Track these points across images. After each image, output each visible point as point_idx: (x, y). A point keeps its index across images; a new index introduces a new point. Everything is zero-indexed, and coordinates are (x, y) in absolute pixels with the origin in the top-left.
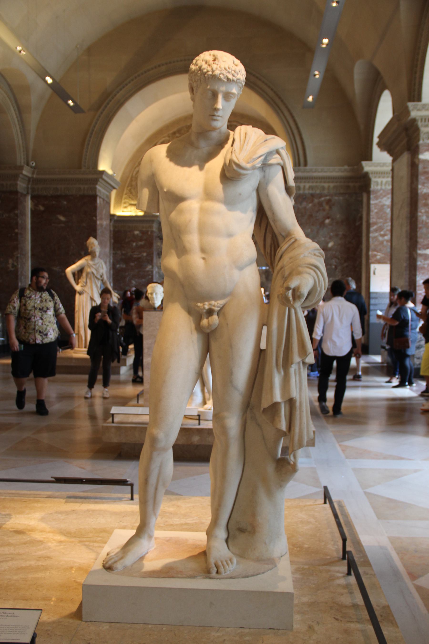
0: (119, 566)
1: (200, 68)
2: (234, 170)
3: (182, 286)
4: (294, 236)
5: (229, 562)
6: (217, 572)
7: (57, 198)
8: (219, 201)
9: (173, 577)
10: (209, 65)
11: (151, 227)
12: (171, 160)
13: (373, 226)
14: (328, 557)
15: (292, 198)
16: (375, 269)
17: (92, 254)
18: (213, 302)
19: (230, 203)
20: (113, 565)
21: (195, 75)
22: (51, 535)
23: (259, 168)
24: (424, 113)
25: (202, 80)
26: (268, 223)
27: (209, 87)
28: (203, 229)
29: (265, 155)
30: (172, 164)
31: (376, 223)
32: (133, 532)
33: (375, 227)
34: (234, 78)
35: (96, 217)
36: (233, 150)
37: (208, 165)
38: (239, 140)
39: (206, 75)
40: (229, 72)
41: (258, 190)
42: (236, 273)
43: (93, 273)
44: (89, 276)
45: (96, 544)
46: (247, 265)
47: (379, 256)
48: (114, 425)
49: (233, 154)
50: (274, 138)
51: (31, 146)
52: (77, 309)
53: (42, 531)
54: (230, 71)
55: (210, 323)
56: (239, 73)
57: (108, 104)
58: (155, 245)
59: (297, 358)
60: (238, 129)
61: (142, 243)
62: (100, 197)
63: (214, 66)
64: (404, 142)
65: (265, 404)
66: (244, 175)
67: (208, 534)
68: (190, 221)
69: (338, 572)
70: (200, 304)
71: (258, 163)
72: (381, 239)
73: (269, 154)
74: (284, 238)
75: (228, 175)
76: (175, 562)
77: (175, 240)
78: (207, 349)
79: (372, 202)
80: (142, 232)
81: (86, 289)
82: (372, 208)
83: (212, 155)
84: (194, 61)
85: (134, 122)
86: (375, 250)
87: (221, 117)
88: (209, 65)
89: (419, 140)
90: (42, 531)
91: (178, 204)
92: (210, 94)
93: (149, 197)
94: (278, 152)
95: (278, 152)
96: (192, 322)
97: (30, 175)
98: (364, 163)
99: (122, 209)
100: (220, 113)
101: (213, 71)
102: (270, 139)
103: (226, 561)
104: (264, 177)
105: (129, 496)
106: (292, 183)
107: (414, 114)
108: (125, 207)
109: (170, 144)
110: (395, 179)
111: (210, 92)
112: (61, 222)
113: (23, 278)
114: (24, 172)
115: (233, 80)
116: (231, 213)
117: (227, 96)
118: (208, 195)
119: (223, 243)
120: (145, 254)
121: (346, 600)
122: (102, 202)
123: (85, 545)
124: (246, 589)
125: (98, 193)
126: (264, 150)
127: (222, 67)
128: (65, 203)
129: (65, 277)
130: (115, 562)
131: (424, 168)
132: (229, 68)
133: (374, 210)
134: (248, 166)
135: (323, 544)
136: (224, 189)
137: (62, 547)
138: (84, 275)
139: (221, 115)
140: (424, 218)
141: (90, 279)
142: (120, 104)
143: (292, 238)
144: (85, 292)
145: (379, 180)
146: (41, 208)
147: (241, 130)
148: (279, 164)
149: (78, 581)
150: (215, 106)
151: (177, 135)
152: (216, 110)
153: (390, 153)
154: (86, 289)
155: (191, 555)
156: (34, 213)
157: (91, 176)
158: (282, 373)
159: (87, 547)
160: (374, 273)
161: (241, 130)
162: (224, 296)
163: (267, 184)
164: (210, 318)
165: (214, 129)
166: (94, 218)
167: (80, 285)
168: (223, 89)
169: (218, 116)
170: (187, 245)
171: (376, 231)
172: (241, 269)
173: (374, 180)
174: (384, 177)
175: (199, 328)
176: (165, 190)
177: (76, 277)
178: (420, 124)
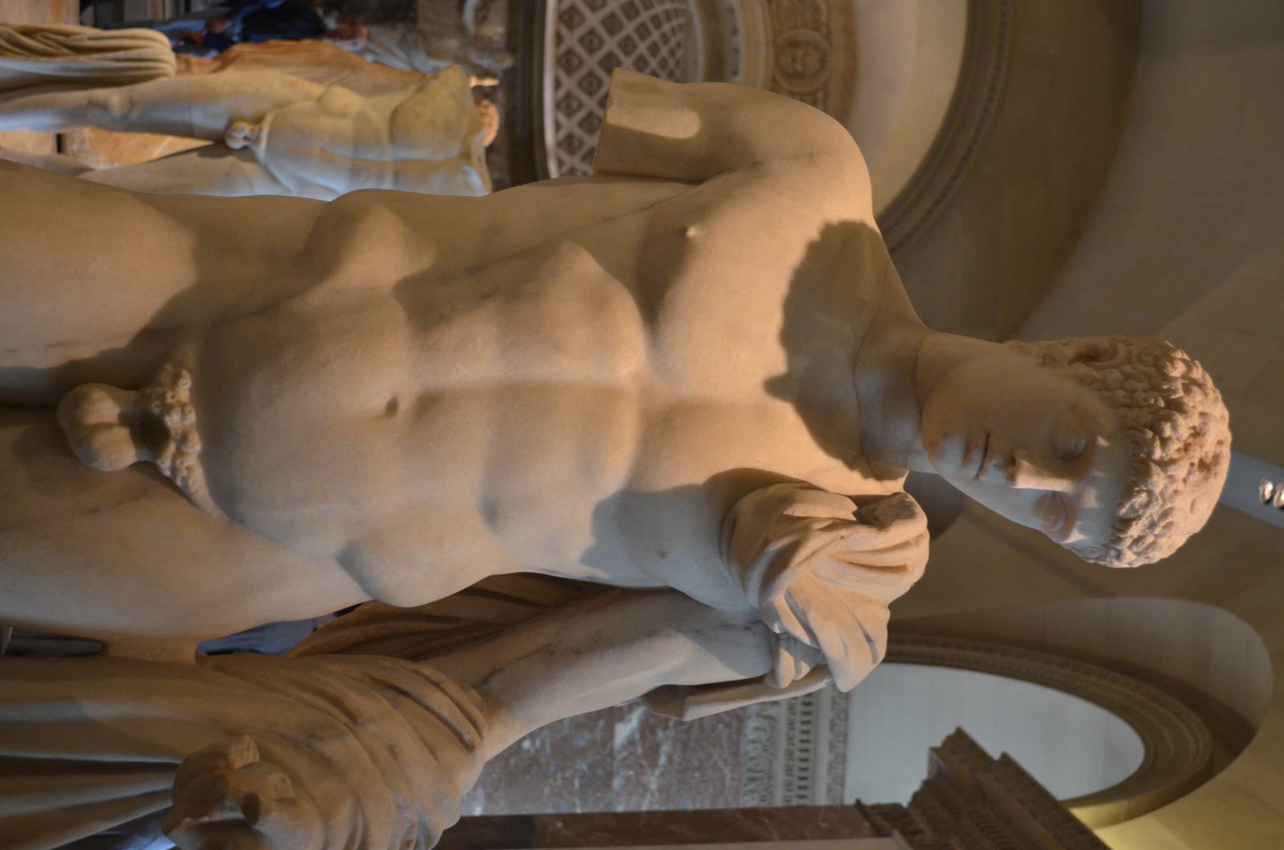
1: (1177, 407)
2: (767, 542)
8: (640, 468)
10: (1186, 448)
12: (814, 249)
18: (195, 446)
19: (629, 512)
21: (1149, 377)
25: (1135, 411)
27: (1102, 442)
28: (520, 404)
30: (794, 255)
34: (1129, 542)
37: (786, 413)
38: (881, 546)
39: (1150, 434)
40: (1152, 525)
42: (333, 542)
46: (361, 580)
54: (1157, 531)
63: (1180, 471)
66: (744, 581)
68: (557, 347)
70: (184, 390)
75: (746, 505)
77: (476, 269)
84: (1198, 373)
87: (978, 475)
88: (1186, 448)
91: (632, 290)
94: (821, 668)
96: (105, 347)
100: (993, 476)
104: (727, 626)
109: (872, 231)
111: (1082, 445)
115: (1119, 540)
116: (584, 515)
118: (666, 422)
119: (461, 484)
134: (779, 600)
136: (687, 492)
139: (982, 478)
150: (1025, 464)
152: (1010, 466)
162: (227, 495)
163: (697, 634)
164: (122, 433)
168: (1091, 500)
169: (982, 468)
170: (451, 335)
172: (348, 560)
176: (692, 232)
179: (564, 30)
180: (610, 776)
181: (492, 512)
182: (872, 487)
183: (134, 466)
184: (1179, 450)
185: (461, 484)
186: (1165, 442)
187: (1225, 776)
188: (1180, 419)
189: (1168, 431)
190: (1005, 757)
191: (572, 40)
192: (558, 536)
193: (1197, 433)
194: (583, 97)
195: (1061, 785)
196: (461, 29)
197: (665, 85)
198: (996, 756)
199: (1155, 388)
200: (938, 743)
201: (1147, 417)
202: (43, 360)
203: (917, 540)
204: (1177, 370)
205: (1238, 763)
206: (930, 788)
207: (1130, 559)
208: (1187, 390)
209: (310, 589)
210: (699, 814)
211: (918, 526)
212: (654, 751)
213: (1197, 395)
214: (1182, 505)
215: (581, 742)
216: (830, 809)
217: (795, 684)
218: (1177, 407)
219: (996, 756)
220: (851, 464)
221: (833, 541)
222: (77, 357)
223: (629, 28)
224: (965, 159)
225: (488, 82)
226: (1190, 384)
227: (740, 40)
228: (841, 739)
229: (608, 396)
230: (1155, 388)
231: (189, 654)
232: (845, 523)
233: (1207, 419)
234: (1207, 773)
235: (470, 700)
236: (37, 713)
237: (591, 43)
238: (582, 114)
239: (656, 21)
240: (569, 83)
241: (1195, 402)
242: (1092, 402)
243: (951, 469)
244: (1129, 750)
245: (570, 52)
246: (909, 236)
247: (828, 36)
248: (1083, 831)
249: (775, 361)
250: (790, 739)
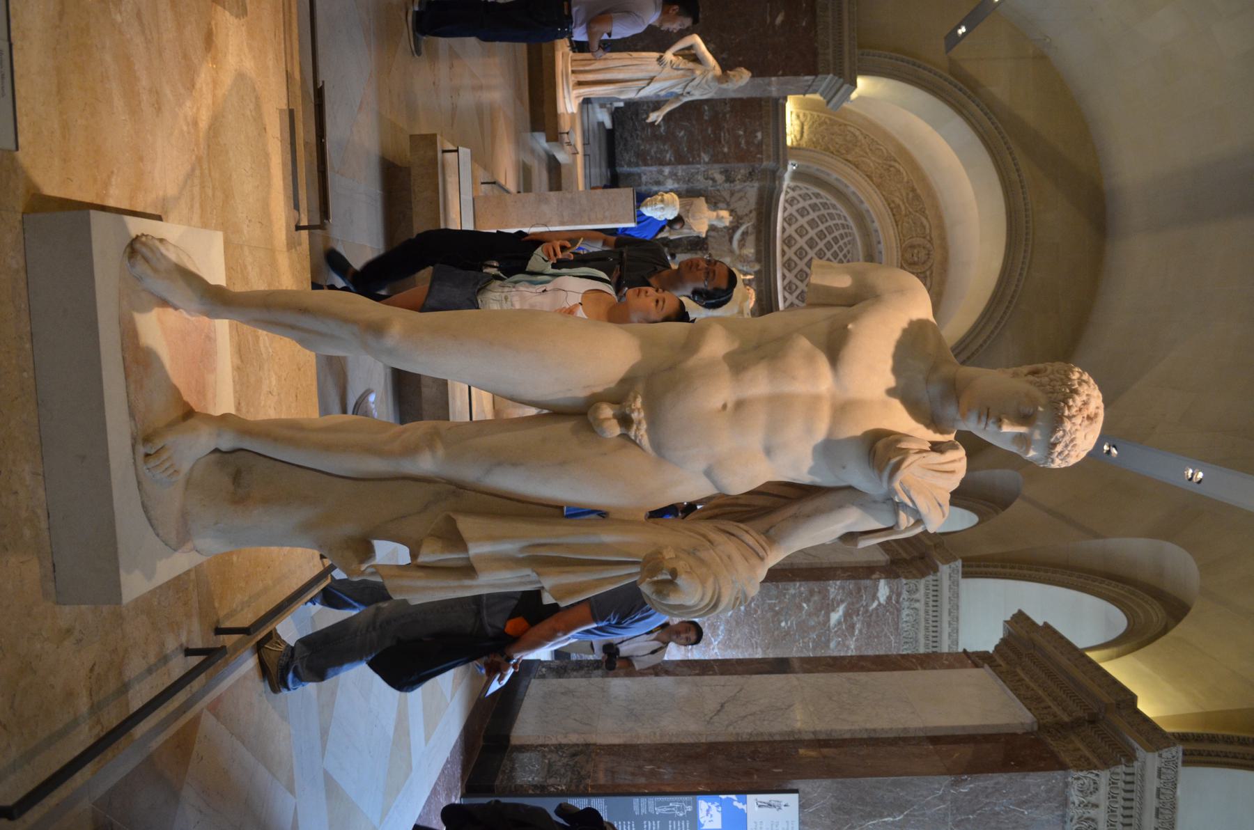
0: (141, 267)
1: (1075, 392)
5: (171, 471)
6: (147, 455)
8: (831, 431)
9: (127, 377)
10: (1080, 410)
11: (768, 157)
12: (906, 332)
14: (217, 605)
17: (724, 78)
18: (644, 426)
19: (829, 449)
20: (139, 257)
22: (208, 100)
24: (946, 583)
27: (1040, 409)
28: (779, 404)
30: (896, 335)
32: (216, 275)
37: (896, 404)
40: (1066, 446)
41: (850, 488)
42: (701, 466)
44: (689, 73)
45: (197, 190)
46: (714, 482)
48: (439, 154)
52: (635, 54)
53: (215, 83)
57: (960, 90)
58: (741, 165)
61: (743, 145)
63: (1078, 420)
64: (904, 555)
65: (466, 525)
66: (880, 478)
67: (225, 417)
68: (794, 378)
69: (189, 632)
74: (766, 533)
75: (880, 444)
76: (162, 367)
77: (758, 347)
78: (556, 413)
80: (761, 143)
84: (1086, 376)
85: (930, 128)
88: (1080, 410)
89: (906, 578)
90: (215, 83)
92: (1027, 410)
93: (836, 289)
94: (919, 521)
99: (795, 111)
100: (992, 427)
101: (1070, 418)
103: (172, 465)
104: (875, 502)
105: (304, 222)
107: (945, 569)
108: (798, 116)
112: (774, 18)
115: (1052, 453)
118: (842, 409)
120: (726, 150)
121: (135, 666)
123: (193, 170)
124: (118, 517)
125: (820, 77)
130: (146, 260)
131: (866, 588)
134: (897, 485)
135: (242, 584)
137: (185, 128)
138: (691, 65)
140: (792, 591)
141: (684, 76)
142: (959, 109)
148: (897, 524)
149: (113, 180)
150: (1006, 421)
151: (911, 195)
152: (999, 422)
154: (668, 68)
155: (182, 391)
157: (846, 64)
158: (521, 556)
159: (190, 175)
163: (862, 506)
164: (615, 422)
167: (673, 58)
168: (1037, 435)
170: (748, 375)
172: (708, 473)
175: (593, 401)
176: (850, 326)
178: (931, 578)
179: (786, 248)
180: (828, 641)
181: (768, 451)
182: (938, 438)
183: (620, 435)
185: (755, 440)
186: (1069, 408)
187: (1173, 633)
188: (1077, 397)
189: (1071, 403)
190: (1045, 623)
191: (790, 253)
192: (796, 463)
193: (1085, 403)
194: (798, 283)
195: (1080, 643)
196: (732, 252)
197: (835, 264)
198: (1040, 623)
199: (1065, 384)
200: (1008, 619)
201: (1061, 397)
202: (581, 393)
203: (960, 459)
204: (1075, 376)
205: (1180, 626)
206: (1005, 643)
207: (1058, 464)
208: (1080, 384)
209: (690, 486)
210: (878, 657)
211: (961, 453)
212: (852, 627)
213: (1085, 386)
214: (1081, 437)
215: (812, 623)
216: (949, 654)
217: (907, 529)
218: (1075, 392)
219: (1040, 623)
220: (928, 426)
223: (821, 245)
224: (1010, 302)
225: (749, 277)
226: (1081, 382)
227: (882, 247)
228: (955, 619)
229: (816, 399)
230: (1065, 384)
232: (926, 451)
233: (1089, 399)
234: (1165, 631)
235: (762, 539)
236: (583, 539)
237: (801, 253)
238: (798, 292)
239: (836, 240)
240: (790, 276)
241: (1084, 389)
242: (1036, 392)
243: (971, 425)
244: (1118, 621)
245: (790, 259)
246: (981, 346)
247: (930, 241)
248: (1091, 661)
249: (890, 381)
250: (926, 620)
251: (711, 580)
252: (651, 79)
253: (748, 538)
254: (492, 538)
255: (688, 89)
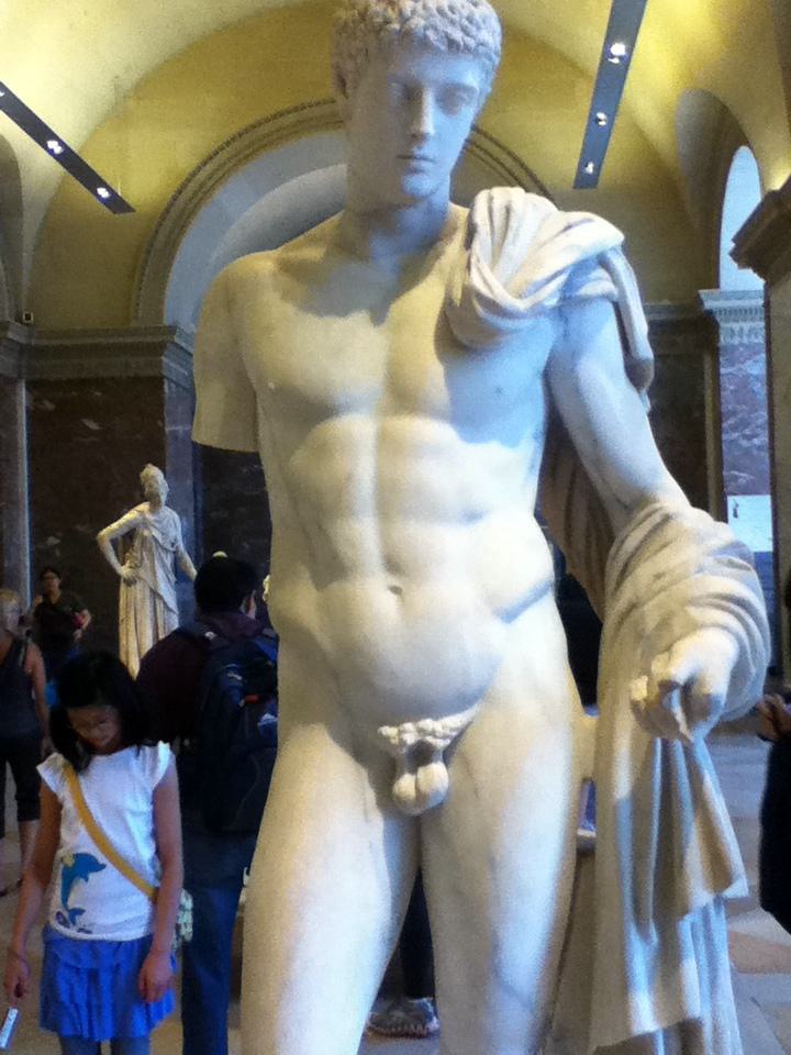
1: (363, 16)
2: (478, 318)
3: (336, 676)
4: (657, 505)
7: (82, 383)
8: (436, 414)
13: (728, 419)
15: (644, 391)
16: (737, 505)
18: (428, 724)
19: (469, 419)
23: (553, 309)
26: (577, 470)
29: (569, 272)
31: (734, 413)
33: (731, 421)
34: (468, 39)
35: (163, 420)
36: (473, 260)
40: (452, 22)
41: (547, 377)
42: (496, 632)
43: (156, 540)
46: (525, 605)
47: (744, 477)
49: (474, 270)
50: (590, 220)
51: (26, 280)
52: (122, 614)
54: (456, 17)
55: (423, 788)
56: (482, 26)
59: (699, 893)
60: (482, 199)
62: (170, 380)
68: (349, 478)
71: (549, 296)
72: (745, 443)
73: (580, 269)
79: (723, 371)
81: (142, 572)
82: (724, 380)
83: (411, 271)
86: (735, 468)
92: (395, 91)
94: (602, 262)
95: (602, 262)
96: (367, 784)
97: (23, 341)
98: (703, 293)
100: (428, 149)
102: (577, 224)
104: (566, 335)
106: (645, 350)
110: (775, 324)
112: (91, 432)
113: (12, 549)
114: (10, 335)
115: (467, 47)
117: (450, 97)
122: (174, 390)
126: (560, 258)
127: (432, 5)
128: (98, 394)
129: (94, 545)
132: (452, 9)
133: (728, 387)
134: (521, 305)
136: (449, 376)
138: (137, 543)
139: (431, 157)
143: (655, 511)
144: (139, 578)
145: (736, 326)
146: (49, 406)
147: (491, 199)
148: (606, 297)
153: (761, 270)
154: (142, 572)
156: (34, 416)
160: (736, 515)
161: (491, 199)
164: (421, 771)
165: (414, 199)
166: (160, 423)
170: (343, 549)
171: (734, 428)
172: (510, 616)
173: (725, 326)
174: (745, 320)
175: (387, 799)
177: (120, 548)
184: (393, 9)
217: (616, 280)
221: (479, 269)
222: (374, 802)
231: (589, 721)
249: (358, 322)
251: (694, 612)
252: (155, 594)
253: (631, 543)
254: (624, 987)
255: (169, 547)
